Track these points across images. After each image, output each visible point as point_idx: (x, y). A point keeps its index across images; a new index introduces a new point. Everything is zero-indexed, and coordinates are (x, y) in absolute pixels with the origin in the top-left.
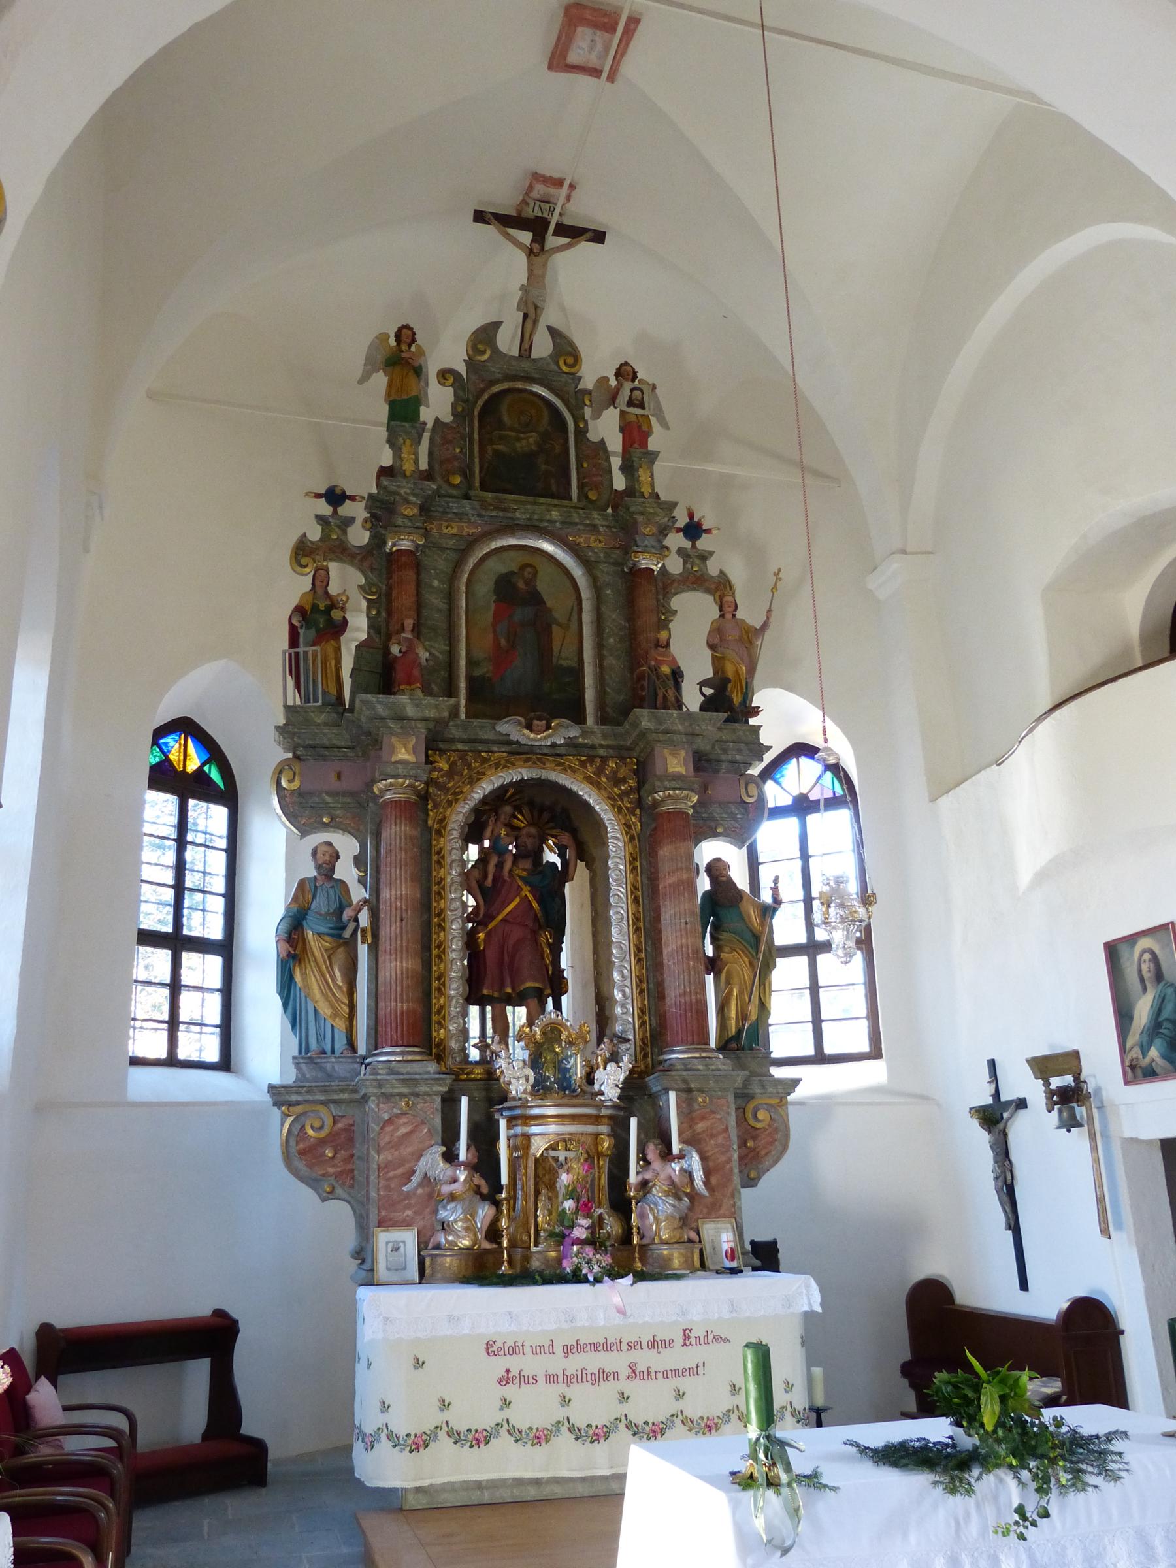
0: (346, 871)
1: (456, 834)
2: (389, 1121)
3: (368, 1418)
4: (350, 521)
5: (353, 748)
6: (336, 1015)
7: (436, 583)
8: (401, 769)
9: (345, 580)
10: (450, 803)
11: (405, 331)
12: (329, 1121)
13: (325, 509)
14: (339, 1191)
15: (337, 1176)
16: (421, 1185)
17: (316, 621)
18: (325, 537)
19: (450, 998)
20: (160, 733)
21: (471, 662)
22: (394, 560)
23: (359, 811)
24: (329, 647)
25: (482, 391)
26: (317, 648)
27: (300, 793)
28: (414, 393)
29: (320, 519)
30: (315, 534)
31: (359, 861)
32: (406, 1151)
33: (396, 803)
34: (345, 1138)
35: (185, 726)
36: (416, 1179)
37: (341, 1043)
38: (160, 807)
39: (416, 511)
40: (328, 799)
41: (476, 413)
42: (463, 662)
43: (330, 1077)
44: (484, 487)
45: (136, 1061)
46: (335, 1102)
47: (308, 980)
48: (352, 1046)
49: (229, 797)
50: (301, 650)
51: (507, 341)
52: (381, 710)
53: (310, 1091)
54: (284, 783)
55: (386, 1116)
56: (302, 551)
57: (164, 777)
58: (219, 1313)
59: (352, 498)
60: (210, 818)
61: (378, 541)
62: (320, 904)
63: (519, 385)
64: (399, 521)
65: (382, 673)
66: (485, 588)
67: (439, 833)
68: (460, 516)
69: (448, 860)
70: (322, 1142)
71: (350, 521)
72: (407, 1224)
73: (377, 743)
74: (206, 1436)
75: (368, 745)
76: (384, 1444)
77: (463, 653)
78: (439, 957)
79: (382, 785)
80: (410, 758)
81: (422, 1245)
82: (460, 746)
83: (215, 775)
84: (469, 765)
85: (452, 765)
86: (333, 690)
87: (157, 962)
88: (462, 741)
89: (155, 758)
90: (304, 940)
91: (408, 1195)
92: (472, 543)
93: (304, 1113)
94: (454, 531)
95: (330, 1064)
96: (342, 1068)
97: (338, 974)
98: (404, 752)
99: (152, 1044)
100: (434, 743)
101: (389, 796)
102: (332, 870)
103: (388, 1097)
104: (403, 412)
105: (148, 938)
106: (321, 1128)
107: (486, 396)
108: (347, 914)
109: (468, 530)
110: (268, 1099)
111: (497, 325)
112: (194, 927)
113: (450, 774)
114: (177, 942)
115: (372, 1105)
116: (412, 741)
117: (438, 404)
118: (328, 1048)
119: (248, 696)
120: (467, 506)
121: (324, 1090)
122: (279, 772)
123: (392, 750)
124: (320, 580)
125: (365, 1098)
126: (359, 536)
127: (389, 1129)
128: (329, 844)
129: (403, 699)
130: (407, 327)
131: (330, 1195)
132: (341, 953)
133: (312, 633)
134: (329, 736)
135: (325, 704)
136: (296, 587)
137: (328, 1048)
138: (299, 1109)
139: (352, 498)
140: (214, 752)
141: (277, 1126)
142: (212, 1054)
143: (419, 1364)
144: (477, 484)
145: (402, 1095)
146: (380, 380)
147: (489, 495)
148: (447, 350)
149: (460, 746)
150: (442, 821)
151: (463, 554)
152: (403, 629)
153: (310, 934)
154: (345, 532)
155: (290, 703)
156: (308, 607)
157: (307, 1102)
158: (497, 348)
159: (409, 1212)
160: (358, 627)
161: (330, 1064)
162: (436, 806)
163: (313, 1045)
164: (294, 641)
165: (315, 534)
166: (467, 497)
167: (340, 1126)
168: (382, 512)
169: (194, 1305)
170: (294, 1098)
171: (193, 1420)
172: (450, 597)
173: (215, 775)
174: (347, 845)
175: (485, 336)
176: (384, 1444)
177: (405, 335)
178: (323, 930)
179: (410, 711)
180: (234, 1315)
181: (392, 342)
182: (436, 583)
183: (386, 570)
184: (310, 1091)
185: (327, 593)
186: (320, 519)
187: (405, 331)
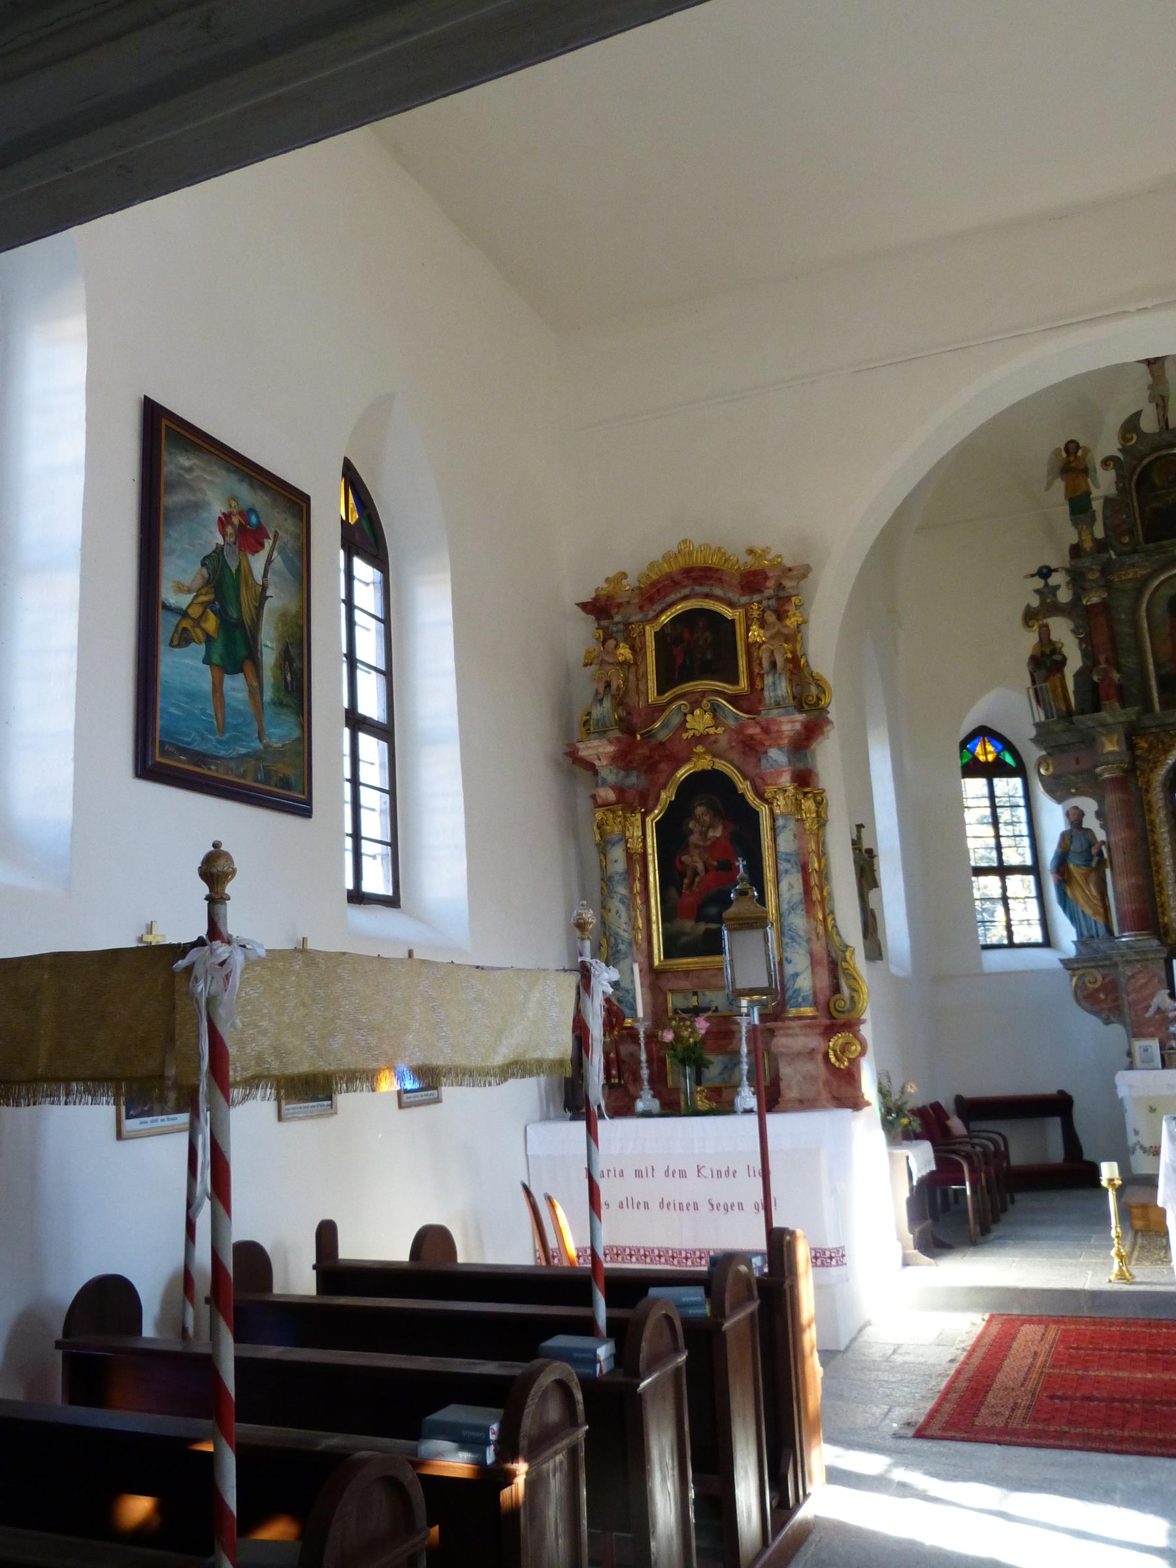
0: (1091, 822)
1: (1159, 789)
2: (1133, 977)
3: (1132, 1140)
4: (1058, 587)
5: (1083, 742)
6: (1095, 913)
7: (1123, 617)
8: (1111, 758)
9: (1062, 630)
10: (1152, 770)
11: (1071, 445)
12: (1100, 979)
13: (1039, 583)
14: (1112, 1018)
15: (1110, 1009)
16: (1156, 1013)
17: (1046, 662)
18: (1043, 602)
19: (1168, 896)
20: (963, 745)
21: (1157, 665)
22: (1089, 609)
23: (1091, 785)
24: (1056, 679)
25: (1135, 468)
26: (1047, 684)
27: (1054, 777)
28: (1084, 489)
29: (1037, 591)
30: (1035, 602)
31: (1099, 815)
32: (1145, 993)
33: (1111, 780)
34: (1111, 987)
35: (983, 732)
36: (1152, 1010)
37: (1102, 930)
38: (975, 787)
39: (1098, 575)
40: (1072, 777)
41: (1133, 486)
42: (1151, 667)
43: (1097, 951)
44: (1148, 540)
45: (986, 947)
46: (1101, 966)
47: (1073, 892)
48: (1109, 931)
49: (1019, 770)
50: (1038, 686)
51: (1149, 424)
52: (1090, 723)
53: (1084, 961)
54: (1043, 771)
55: (1130, 974)
56: (1030, 616)
57: (973, 769)
58: (1061, 1093)
59: (1056, 570)
60: (1009, 787)
61: (1077, 599)
62: (1076, 847)
63: (1164, 452)
64: (1088, 585)
65: (1093, 695)
66: (1161, 610)
67: (1147, 791)
68: (1133, 565)
69: (1156, 807)
70: (1098, 990)
71: (1058, 587)
72: (1152, 1036)
73: (1093, 740)
74: (1065, 1161)
75: (1089, 741)
76: (1139, 1152)
77: (1150, 660)
78: (1158, 872)
79: (1099, 770)
80: (1115, 748)
81: (1162, 1047)
82: (1153, 730)
83: (1009, 759)
84: (1162, 742)
85: (1151, 745)
86: (1063, 708)
87: (989, 885)
88: (1156, 727)
89: (967, 757)
90: (1068, 870)
91: (1150, 1019)
92: (1144, 581)
93: (1083, 975)
94: (1131, 576)
95: (1096, 943)
96: (1104, 946)
97: (1093, 889)
98: (1111, 746)
99: (997, 934)
100: (1132, 734)
101: (1106, 776)
102: (1080, 822)
103: (1128, 962)
104: (1079, 506)
105: (979, 871)
106: (1095, 982)
107: (1139, 470)
108: (1094, 851)
109: (1141, 572)
110: (1061, 966)
111: (1138, 415)
112: (1012, 857)
113: (1149, 750)
114: (1003, 870)
115: (1120, 968)
116: (1115, 738)
117: (1103, 484)
118: (1094, 933)
119: (1013, 708)
120: (1136, 557)
121: (1093, 960)
122: (1039, 766)
123: (1103, 745)
124: (1045, 632)
125: (1116, 965)
126: (1064, 596)
127: (1133, 981)
128: (1076, 808)
129: (1103, 714)
130: (1072, 442)
131: (1107, 1022)
132: (1093, 877)
133: (1044, 671)
134: (1066, 738)
135: (1059, 718)
136: (1029, 641)
137: (1094, 933)
138: (1080, 972)
139: (1056, 570)
140: (1007, 745)
141: (1067, 983)
142: (1036, 935)
143: (1152, 1110)
144: (1141, 539)
145: (1138, 961)
146: (1060, 485)
147: (1151, 546)
148: (1107, 444)
149: (1153, 730)
150: (1148, 783)
151: (1140, 591)
152: (1099, 663)
153: (1071, 866)
154: (1055, 595)
155: (1037, 720)
156: (1039, 655)
157: (1083, 968)
158: (1142, 431)
159: (1152, 1029)
160: (1074, 662)
161: (1096, 943)
162: (1143, 772)
163: (1085, 933)
164: (1034, 682)
165: (1035, 602)
166: (1136, 552)
167: (1107, 980)
168: (1077, 578)
169: (1047, 1087)
170: (1076, 966)
171: (1056, 1153)
172: (1135, 623)
173: (1009, 759)
174: (1089, 805)
175: (1131, 425)
176: (1139, 1152)
177: (1072, 447)
178: (1078, 862)
179: (1109, 720)
180: (1071, 1093)
181: (1064, 455)
182: (1123, 617)
183: (1087, 620)
184: (1084, 961)
185: (1050, 640)
186: (1037, 591)
187: (1071, 445)
